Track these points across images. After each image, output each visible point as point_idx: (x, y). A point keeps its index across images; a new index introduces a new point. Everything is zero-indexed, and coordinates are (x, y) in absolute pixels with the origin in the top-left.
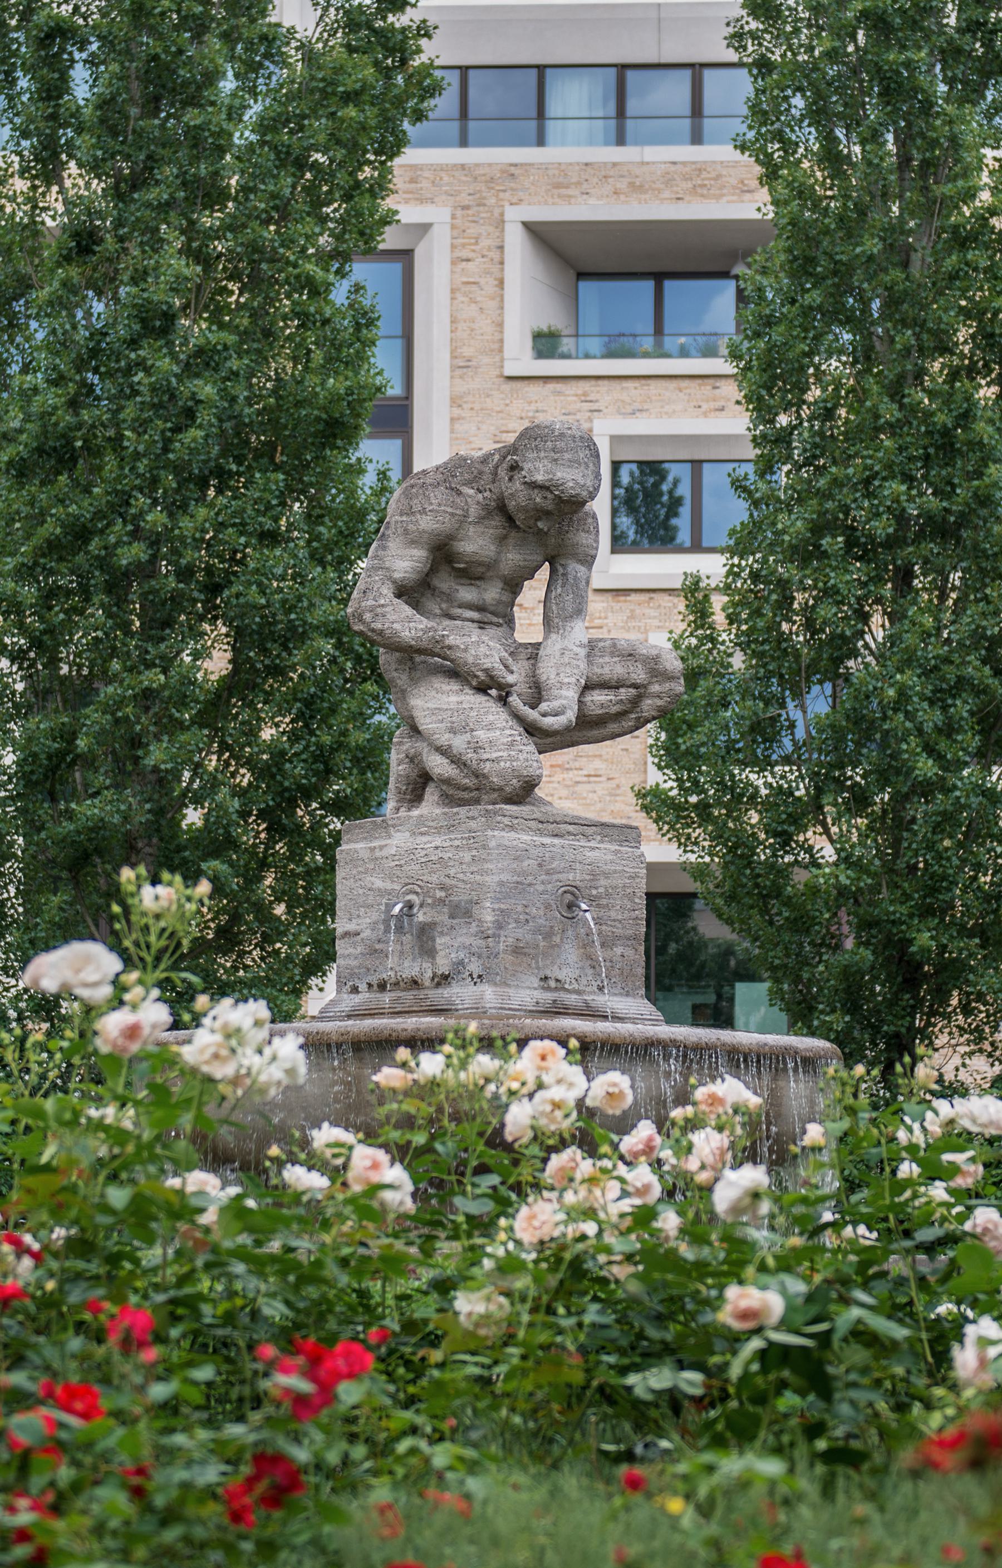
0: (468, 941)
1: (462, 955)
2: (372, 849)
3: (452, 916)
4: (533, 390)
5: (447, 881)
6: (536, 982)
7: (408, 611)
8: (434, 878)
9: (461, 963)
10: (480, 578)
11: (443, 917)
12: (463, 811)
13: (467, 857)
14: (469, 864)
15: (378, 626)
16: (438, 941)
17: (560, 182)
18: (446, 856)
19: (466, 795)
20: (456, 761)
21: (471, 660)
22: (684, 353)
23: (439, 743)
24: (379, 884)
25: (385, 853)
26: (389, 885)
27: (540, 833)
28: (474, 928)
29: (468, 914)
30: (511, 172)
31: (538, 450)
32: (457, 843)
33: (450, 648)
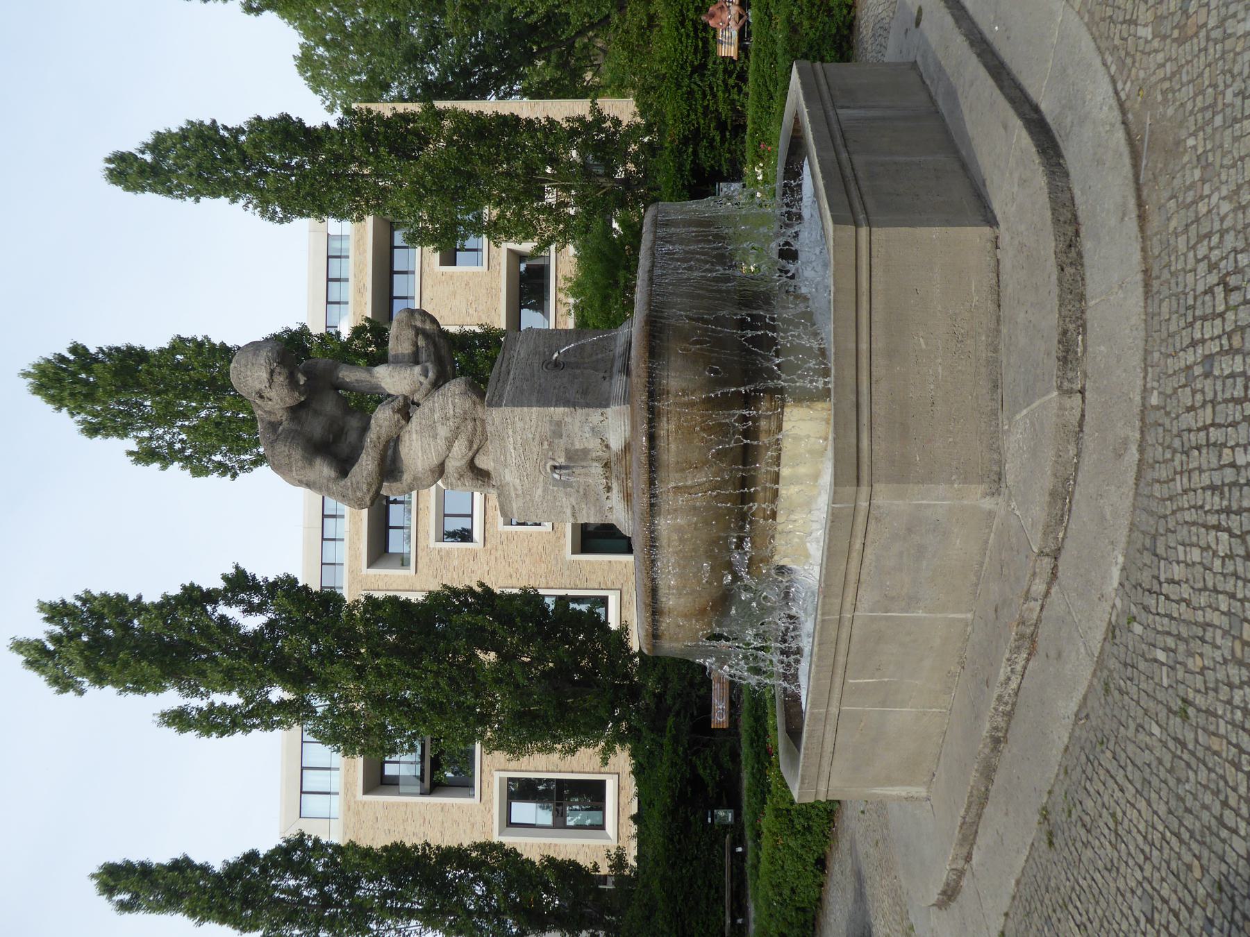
0: (578, 424)
1: (587, 429)
2: (517, 496)
3: (561, 436)
4: (420, 566)
5: (537, 439)
6: (606, 383)
7: (356, 468)
8: (535, 450)
9: (593, 429)
10: (342, 429)
11: (562, 443)
12: (489, 429)
13: (519, 424)
14: (525, 423)
15: (365, 487)
16: (578, 447)
17: (354, 557)
18: (520, 441)
19: (479, 429)
20: (455, 435)
21: (387, 423)
22: (410, 519)
23: (444, 448)
24: (540, 492)
25: (519, 487)
26: (541, 485)
27: (505, 382)
28: (568, 420)
29: (559, 424)
30: (351, 572)
31: (246, 376)
32: (510, 433)
33: (379, 438)
